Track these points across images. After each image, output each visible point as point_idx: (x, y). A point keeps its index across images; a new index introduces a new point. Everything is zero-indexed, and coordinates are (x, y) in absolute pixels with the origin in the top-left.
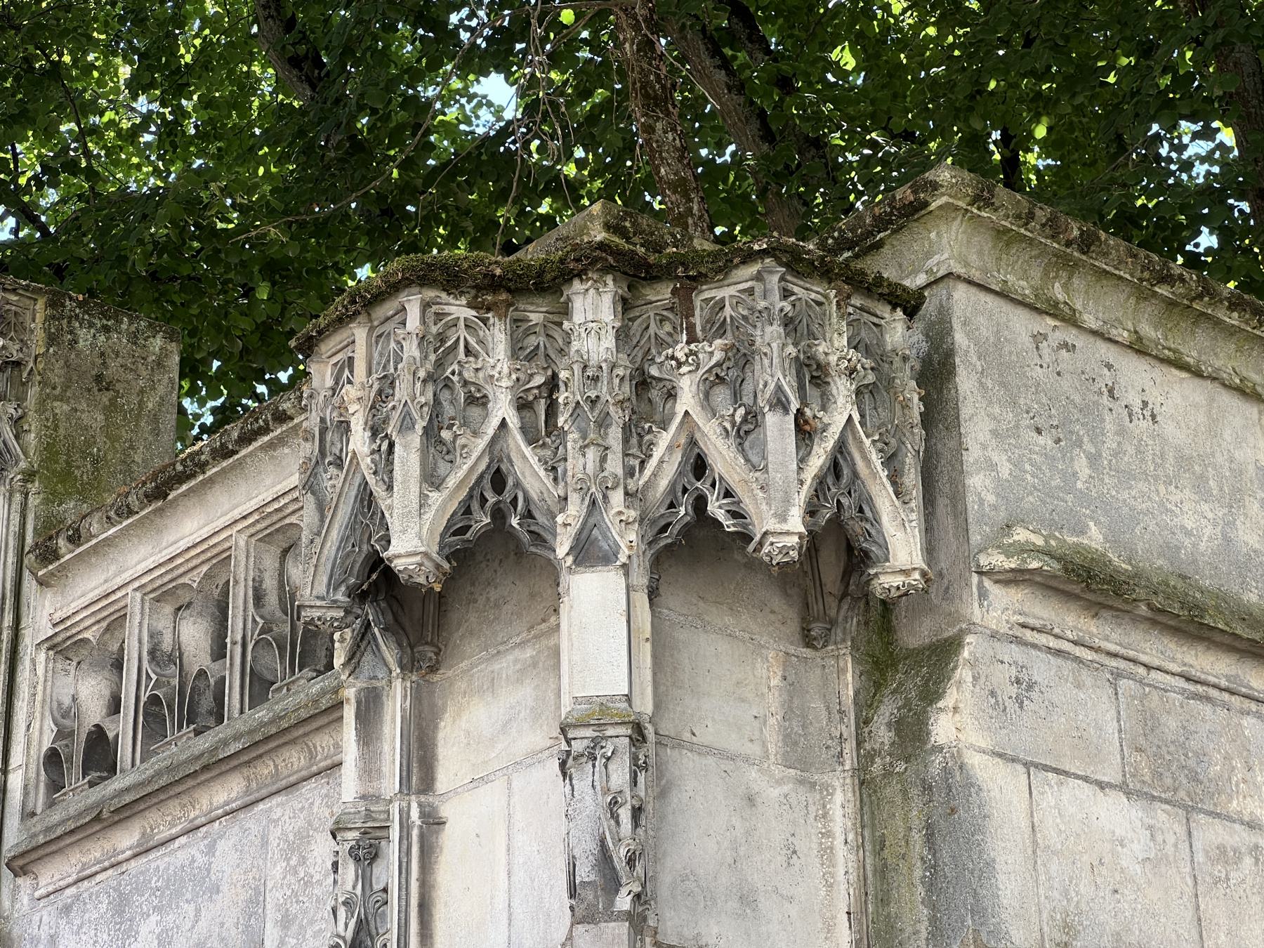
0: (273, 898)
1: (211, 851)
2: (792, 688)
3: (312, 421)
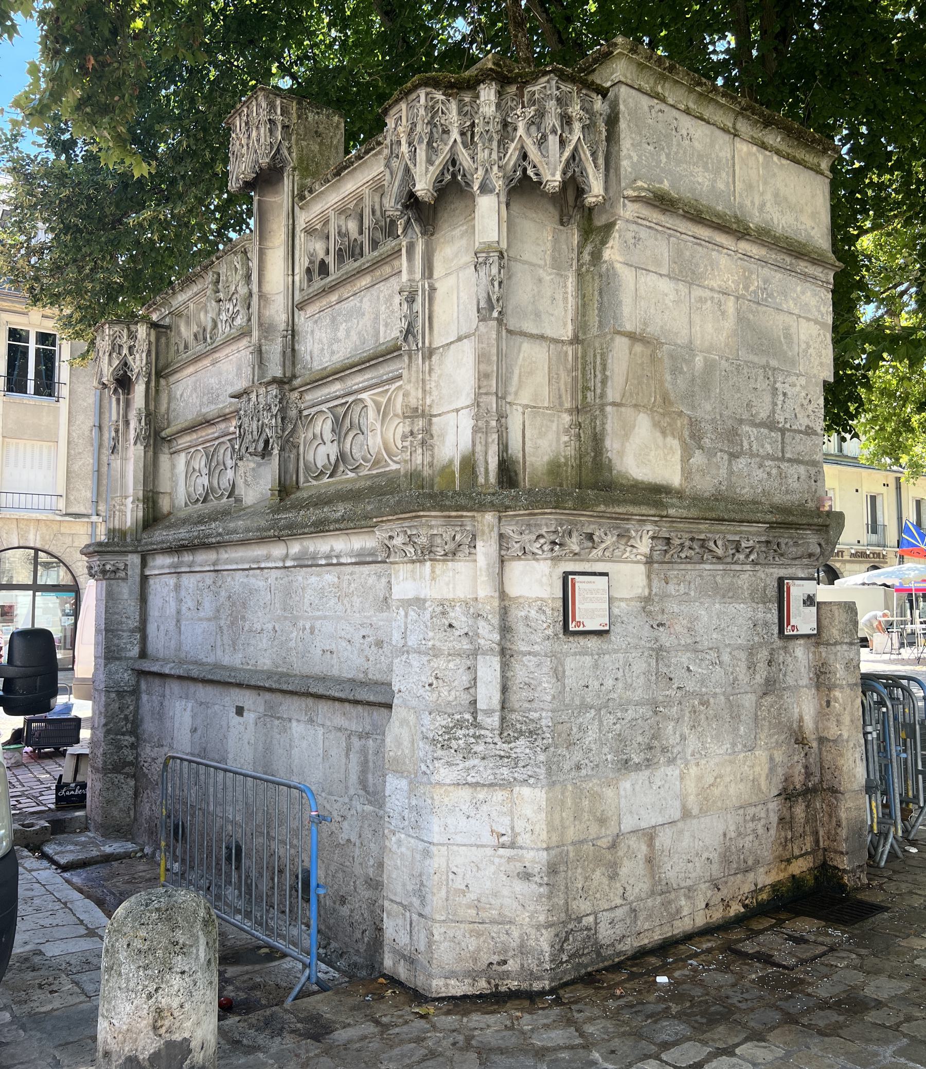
0: (382, 317)
1: (361, 301)
2: (556, 241)
3: (388, 141)
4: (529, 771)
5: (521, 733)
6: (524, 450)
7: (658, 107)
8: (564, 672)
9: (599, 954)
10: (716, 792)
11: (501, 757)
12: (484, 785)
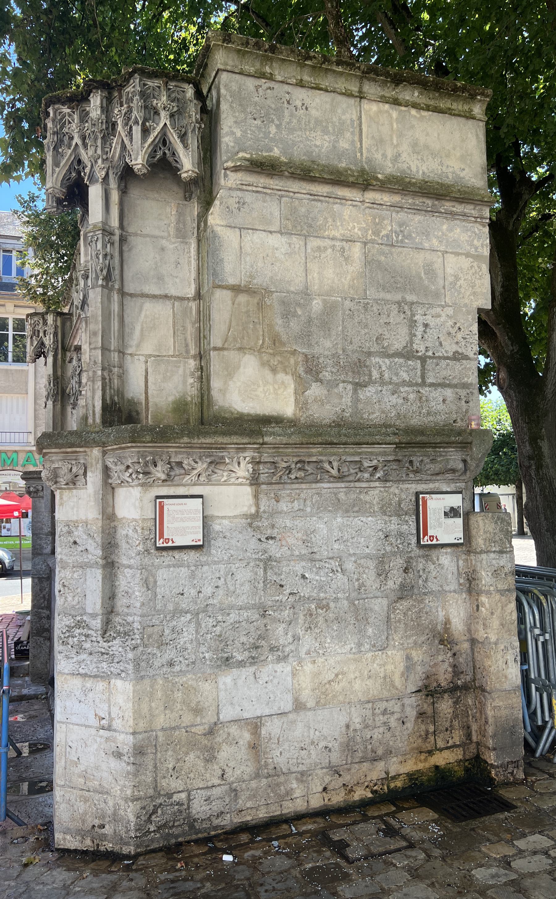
4: (122, 666)
5: (119, 633)
6: (146, 393)
7: (267, 85)
8: (155, 582)
9: (192, 826)
10: (337, 687)
11: (103, 654)
12: (90, 676)
